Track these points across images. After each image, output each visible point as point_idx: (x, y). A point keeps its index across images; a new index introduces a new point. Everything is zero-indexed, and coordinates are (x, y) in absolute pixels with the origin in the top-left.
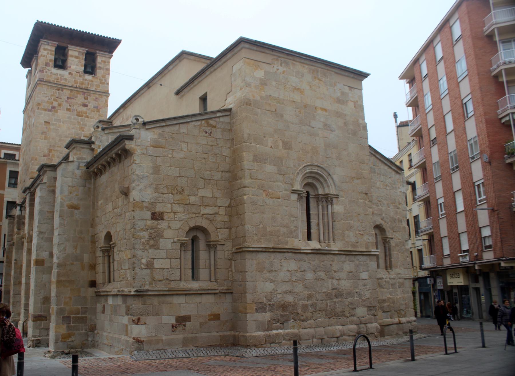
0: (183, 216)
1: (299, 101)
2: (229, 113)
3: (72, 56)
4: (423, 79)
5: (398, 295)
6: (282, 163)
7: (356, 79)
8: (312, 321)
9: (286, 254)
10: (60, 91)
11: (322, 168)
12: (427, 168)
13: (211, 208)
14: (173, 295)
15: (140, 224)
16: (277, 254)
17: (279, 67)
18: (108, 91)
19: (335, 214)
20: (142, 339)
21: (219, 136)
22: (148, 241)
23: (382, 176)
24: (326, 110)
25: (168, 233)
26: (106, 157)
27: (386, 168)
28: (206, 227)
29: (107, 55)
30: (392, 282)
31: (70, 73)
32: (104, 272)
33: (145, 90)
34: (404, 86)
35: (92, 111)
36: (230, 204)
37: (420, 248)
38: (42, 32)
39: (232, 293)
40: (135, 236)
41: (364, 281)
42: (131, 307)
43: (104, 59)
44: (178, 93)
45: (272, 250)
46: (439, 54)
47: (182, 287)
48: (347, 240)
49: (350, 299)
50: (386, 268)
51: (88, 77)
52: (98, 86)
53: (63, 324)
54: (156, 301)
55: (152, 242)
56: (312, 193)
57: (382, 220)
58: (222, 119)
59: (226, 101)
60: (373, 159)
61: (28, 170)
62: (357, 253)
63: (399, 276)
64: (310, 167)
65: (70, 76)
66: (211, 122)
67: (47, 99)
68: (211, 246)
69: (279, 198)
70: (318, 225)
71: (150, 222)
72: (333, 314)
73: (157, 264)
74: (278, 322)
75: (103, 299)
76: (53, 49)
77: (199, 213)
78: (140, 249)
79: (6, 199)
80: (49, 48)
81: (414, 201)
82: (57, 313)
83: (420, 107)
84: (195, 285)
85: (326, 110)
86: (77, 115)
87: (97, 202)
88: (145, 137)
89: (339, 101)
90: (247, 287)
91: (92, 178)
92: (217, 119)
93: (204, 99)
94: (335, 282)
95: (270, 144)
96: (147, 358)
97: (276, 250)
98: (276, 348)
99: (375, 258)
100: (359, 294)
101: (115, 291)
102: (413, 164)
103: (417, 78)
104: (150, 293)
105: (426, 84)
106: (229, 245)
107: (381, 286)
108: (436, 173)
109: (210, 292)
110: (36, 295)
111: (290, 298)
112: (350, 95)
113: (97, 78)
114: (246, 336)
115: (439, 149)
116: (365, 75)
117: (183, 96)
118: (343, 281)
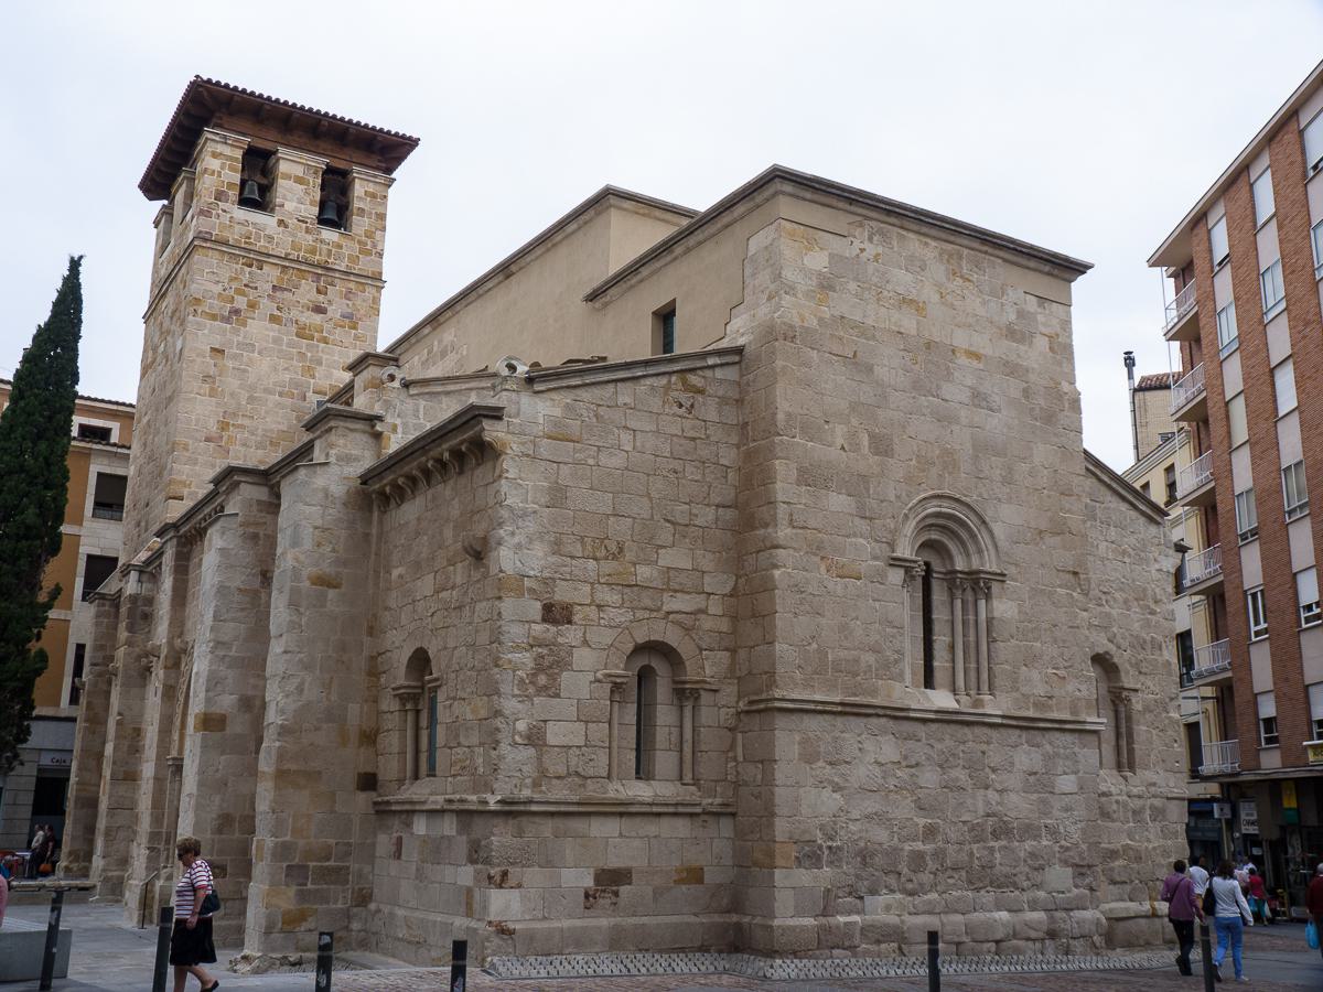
0: (621, 616)
1: (914, 332)
2: (737, 358)
3: (288, 177)
4: (1218, 268)
5: (1149, 841)
6: (868, 490)
7: (1056, 277)
8: (933, 896)
9: (874, 721)
10: (254, 268)
11: (968, 505)
12: (1220, 507)
13: (687, 597)
14: (589, 814)
15: (515, 632)
16: (851, 718)
17: (866, 245)
18: (381, 273)
19: (995, 622)
20: (511, 926)
21: (712, 415)
22: (534, 675)
23: (1112, 528)
24: (977, 357)
25: (584, 658)
26: (424, 459)
27: (1124, 507)
28: (675, 645)
29: (381, 177)
30: (1135, 804)
31: (281, 222)
32: (403, 753)
33: (496, 281)
34: (1161, 285)
35: (337, 325)
36: (735, 588)
37: (1192, 719)
38: (207, 106)
39: (733, 815)
40: (500, 663)
41: (1067, 799)
42: (483, 843)
43: (371, 188)
44: (592, 297)
45: (840, 709)
46: (1266, 204)
47: (611, 794)
48: (1024, 690)
49: (1029, 845)
50: (1119, 767)
51: (330, 235)
52: (354, 259)
53: (287, 885)
54: (547, 828)
55: (542, 680)
56: (937, 566)
57: (1109, 640)
58: (719, 373)
59: (728, 327)
60: (1090, 482)
61: (160, 475)
62: (1049, 725)
63: (1152, 789)
64: (935, 502)
65: (281, 229)
66: (693, 379)
67: (218, 289)
68: (685, 694)
69: (859, 579)
70: (952, 647)
71: (538, 629)
72: (982, 877)
73: (555, 735)
74: (850, 894)
75: (396, 822)
76: (239, 154)
77: (659, 610)
78: (514, 696)
79: (85, 550)
80: (227, 151)
81: (1177, 594)
82: (274, 855)
83: (1204, 342)
84: (642, 791)
85: (977, 357)
86: (297, 335)
87: (389, 572)
88: (531, 415)
89: (1011, 333)
90: (777, 801)
91: (375, 508)
92: (708, 373)
93: (665, 317)
94: (992, 795)
95: (840, 441)
96: (525, 974)
97: (848, 709)
98: (846, 961)
99: (1094, 738)
100: (1053, 832)
101: (437, 801)
102: (1179, 495)
103: (1200, 265)
104: (534, 808)
105: (1224, 285)
106: (729, 692)
107: (1105, 815)
108: (1246, 520)
109: (681, 809)
110: (199, 808)
111: (881, 835)
112: (1040, 318)
113: (353, 239)
114: (771, 927)
115: (1253, 457)
116: (1079, 268)
117: (606, 305)
118: (1013, 797)
